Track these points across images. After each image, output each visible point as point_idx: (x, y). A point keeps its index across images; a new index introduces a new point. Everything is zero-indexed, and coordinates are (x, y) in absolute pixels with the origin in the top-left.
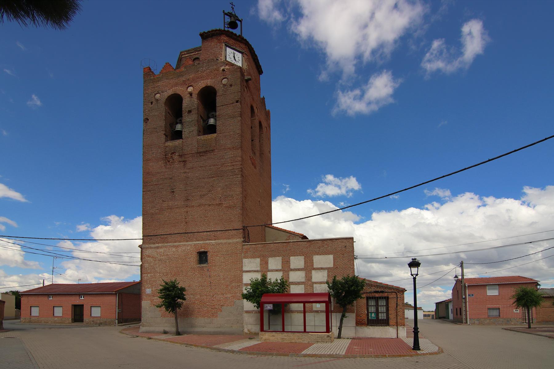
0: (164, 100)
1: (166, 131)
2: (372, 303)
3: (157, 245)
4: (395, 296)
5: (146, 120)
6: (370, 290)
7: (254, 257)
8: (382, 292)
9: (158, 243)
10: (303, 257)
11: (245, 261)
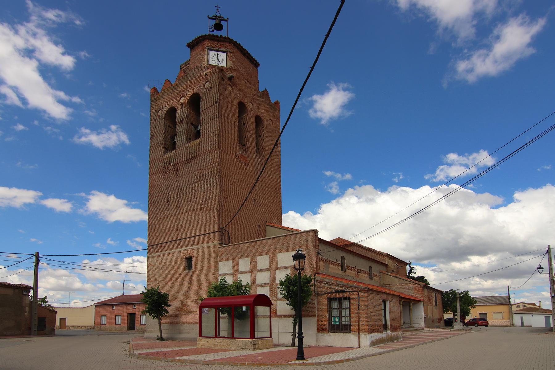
0: (164, 115)
1: (165, 144)
2: (335, 305)
3: (157, 254)
4: (357, 296)
5: (152, 137)
6: (331, 289)
7: (227, 260)
8: (343, 291)
9: (158, 252)
10: (268, 256)
11: (221, 264)
